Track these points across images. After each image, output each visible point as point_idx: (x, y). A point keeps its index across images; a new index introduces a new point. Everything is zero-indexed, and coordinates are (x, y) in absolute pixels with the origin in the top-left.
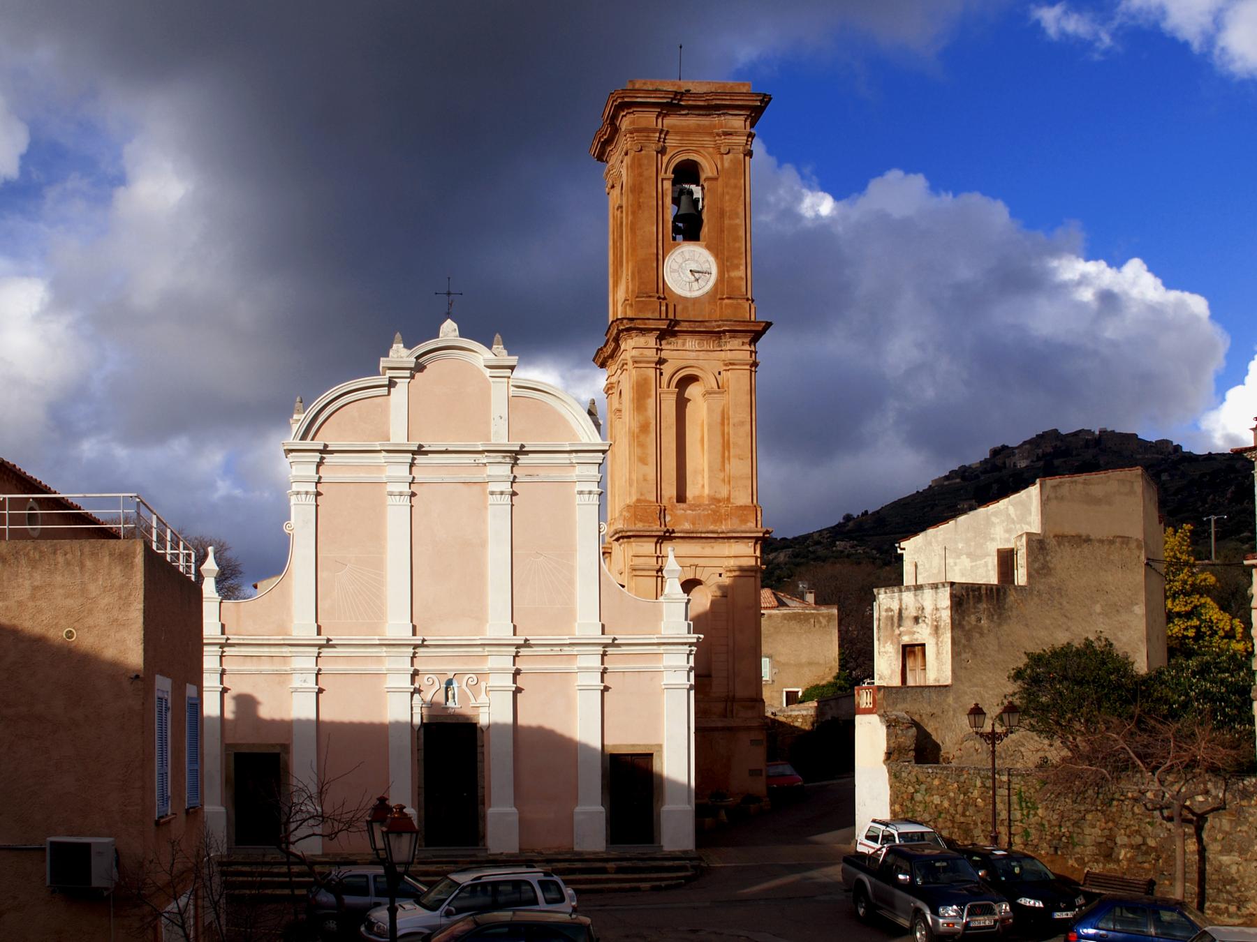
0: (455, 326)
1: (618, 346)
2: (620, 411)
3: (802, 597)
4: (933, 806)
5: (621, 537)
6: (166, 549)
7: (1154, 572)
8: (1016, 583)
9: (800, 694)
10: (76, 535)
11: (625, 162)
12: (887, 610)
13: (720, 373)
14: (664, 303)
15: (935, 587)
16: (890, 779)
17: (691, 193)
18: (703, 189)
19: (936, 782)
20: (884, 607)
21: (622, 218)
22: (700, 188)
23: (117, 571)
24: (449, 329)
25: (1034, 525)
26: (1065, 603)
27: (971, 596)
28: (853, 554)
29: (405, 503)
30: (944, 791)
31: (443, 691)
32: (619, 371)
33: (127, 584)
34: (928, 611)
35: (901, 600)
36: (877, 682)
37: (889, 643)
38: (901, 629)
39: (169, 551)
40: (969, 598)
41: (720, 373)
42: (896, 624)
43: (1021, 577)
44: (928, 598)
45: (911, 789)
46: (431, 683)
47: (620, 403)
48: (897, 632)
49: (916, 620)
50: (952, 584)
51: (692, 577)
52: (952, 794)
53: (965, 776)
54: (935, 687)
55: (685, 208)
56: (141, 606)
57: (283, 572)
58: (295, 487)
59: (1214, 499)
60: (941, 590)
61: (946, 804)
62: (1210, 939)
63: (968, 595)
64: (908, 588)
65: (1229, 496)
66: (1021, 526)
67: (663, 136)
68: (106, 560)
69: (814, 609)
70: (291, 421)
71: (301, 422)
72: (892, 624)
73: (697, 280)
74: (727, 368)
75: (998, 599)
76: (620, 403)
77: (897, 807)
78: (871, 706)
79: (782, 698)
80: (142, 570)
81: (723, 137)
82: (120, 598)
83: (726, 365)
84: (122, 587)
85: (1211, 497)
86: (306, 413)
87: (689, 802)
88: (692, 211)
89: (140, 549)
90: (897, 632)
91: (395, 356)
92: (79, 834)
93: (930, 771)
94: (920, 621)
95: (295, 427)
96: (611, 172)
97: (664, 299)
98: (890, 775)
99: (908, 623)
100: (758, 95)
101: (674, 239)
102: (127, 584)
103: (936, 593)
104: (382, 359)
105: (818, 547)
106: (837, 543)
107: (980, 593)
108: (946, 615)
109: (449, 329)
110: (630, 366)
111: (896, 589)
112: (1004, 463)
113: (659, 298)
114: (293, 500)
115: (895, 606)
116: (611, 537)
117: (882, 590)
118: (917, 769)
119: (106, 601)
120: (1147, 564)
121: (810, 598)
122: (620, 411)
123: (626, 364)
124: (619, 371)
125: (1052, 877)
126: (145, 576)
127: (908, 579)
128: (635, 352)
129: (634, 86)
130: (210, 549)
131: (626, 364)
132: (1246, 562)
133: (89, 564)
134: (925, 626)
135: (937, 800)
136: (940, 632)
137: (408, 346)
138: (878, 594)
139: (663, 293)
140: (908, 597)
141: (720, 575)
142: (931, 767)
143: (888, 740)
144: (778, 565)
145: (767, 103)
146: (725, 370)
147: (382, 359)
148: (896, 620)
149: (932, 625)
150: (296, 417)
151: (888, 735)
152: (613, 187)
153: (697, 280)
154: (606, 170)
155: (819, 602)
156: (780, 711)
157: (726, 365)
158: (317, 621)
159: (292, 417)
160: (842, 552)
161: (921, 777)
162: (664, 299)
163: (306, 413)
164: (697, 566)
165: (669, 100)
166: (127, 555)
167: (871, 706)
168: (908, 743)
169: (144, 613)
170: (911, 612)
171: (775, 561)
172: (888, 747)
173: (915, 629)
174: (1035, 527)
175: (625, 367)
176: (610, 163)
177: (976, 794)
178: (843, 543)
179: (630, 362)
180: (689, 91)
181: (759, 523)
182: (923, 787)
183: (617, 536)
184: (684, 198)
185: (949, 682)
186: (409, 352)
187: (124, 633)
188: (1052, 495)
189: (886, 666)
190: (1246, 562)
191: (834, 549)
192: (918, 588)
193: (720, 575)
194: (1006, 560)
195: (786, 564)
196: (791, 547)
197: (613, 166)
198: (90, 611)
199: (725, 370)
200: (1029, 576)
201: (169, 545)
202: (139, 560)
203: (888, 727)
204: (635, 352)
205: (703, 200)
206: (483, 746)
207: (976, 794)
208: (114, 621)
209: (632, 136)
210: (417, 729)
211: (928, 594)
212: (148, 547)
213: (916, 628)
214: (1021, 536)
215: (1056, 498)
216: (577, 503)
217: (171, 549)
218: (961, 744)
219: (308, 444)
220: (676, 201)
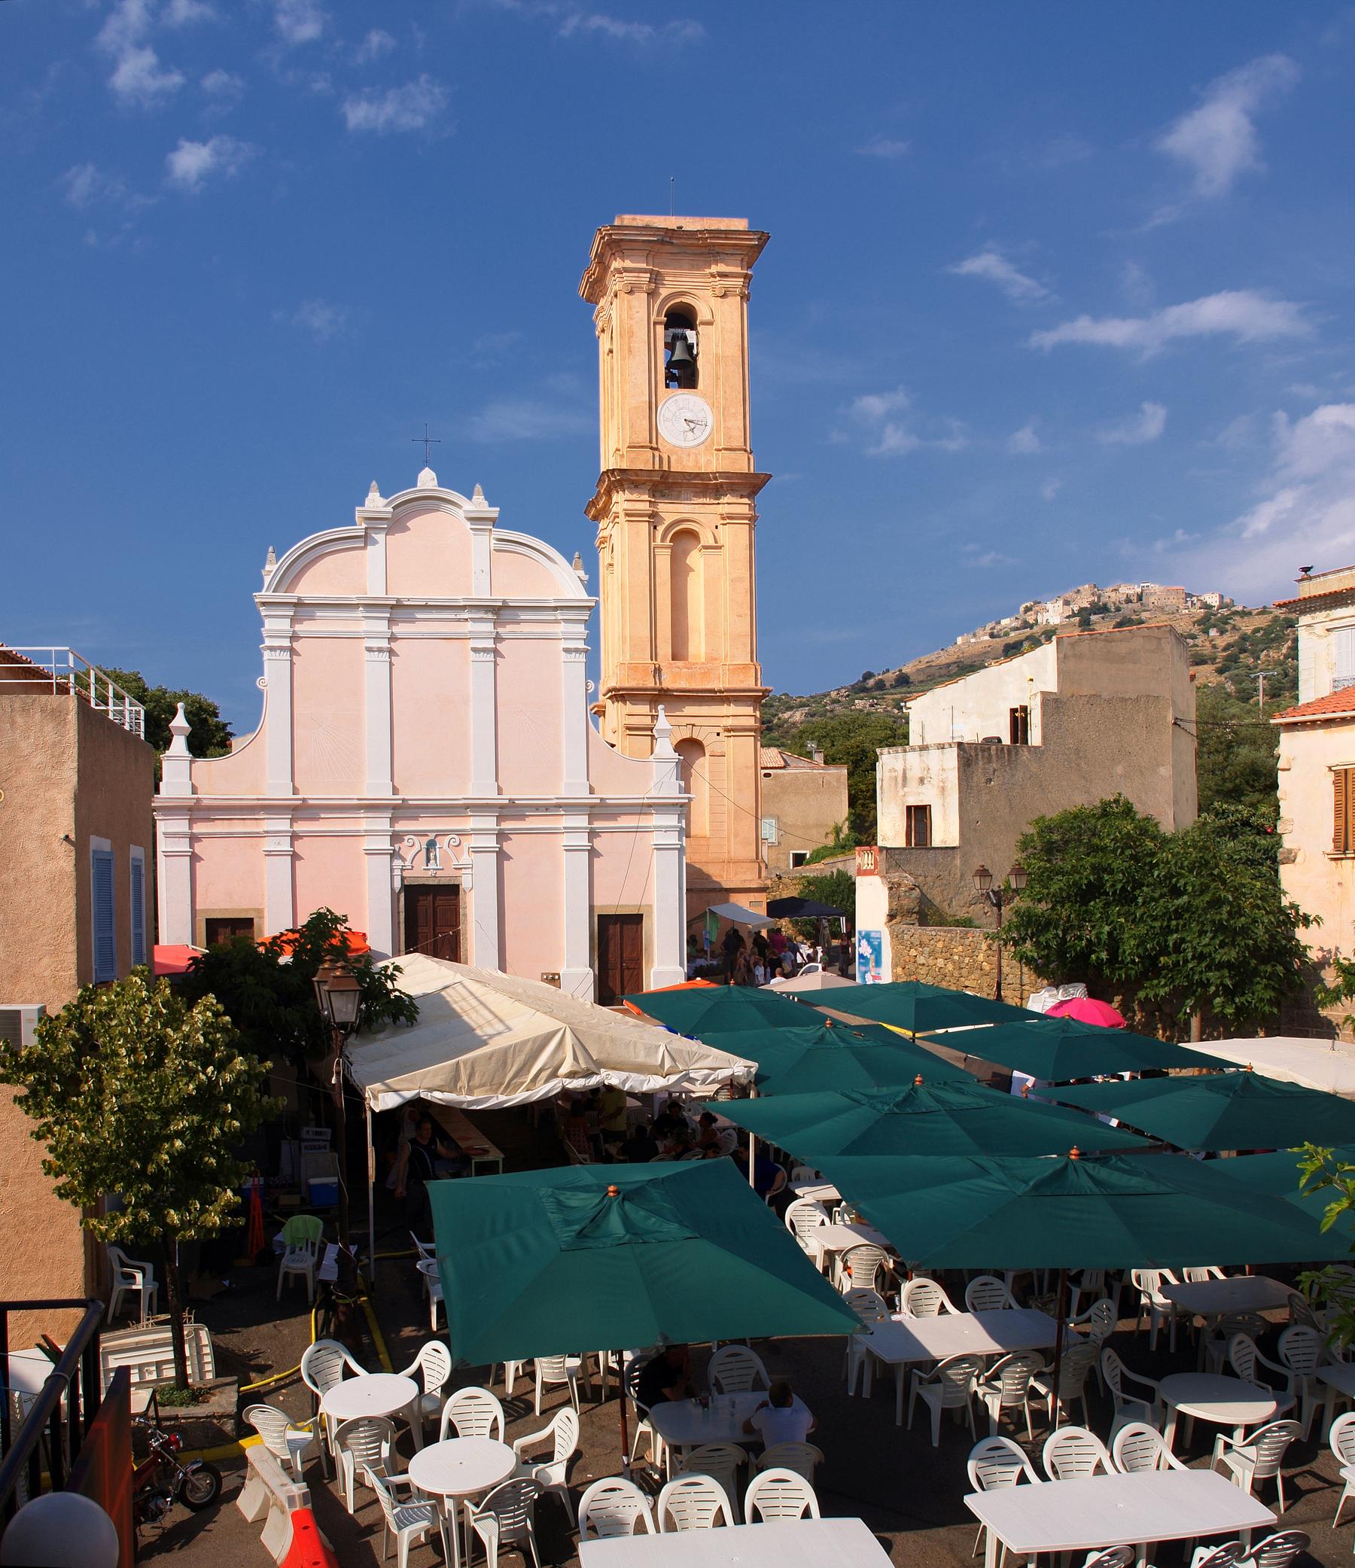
0: (433, 475)
1: (610, 498)
2: (611, 565)
3: (809, 755)
4: (937, 969)
5: (620, 695)
6: (107, 704)
7: (1183, 732)
8: (1030, 744)
9: (808, 856)
10: (27, 689)
11: (614, 304)
12: (890, 771)
13: (717, 527)
14: (657, 453)
15: (942, 747)
16: (892, 941)
17: (685, 338)
18: (697, 334)
19: (940, 945)
20: (887, 768)
21: (612, 363)
22: (694, 332)
23: (49, 728)
24: (427, 479)
25: (1051, 684)
26: (1083, 765)
27: (980, 757)
28: (873, 713)
29: (383, 659)
30: (948, 954)
31: (424, 851)
32: (611, 525)
33: (60, 741)
34: (933, 773)
35: (905, 760)
36: (880, 843)
37: (893, 805)
38: (906, 789)
39: (111, 707)
40: (977, 759)
41: (717, 527)
42: (900, 785)
43: (1035, 737)
44: (933, 756)
45: (913, 952)
46: (410, 844)
47: (612, 558)
48: (901, 793)
49: (922, 781)
50: (960, 744)
51: (688, 736)
52: (956, 957)
53: (971, 939)
54: (941, 848)
55: (679, 354)
56: (76, 764)
57: (255, 730)
58: (268, 642)
59: (1267, 655)
60: (948, 751)
61: (950, 967)
62: (1002, 1417)
63: (977, 755)
64: (913, 749)
65: (1284, 651)
66: (172, 810)
67: (654, 276)
68: (38, 716)
69: (823, 768)
70: (263, 573)
71: (272, 574)
72: (896, 784)
73: (692, 430)
74: (725, 522)
75: (1009, 760)
76: (612, 558)
77: (899, 970)
78: (873, 868)
79: (788, 860)
80: (76, 727)
81: (718, 278)
82: (53, 756)
83: (723, 519)
84: (54, 744)
85: (1265, 652)
86: (279, 564)
87: (681, 964)
88: (687, 357)
89: (71, 702)
90: (901, 793)
91: (372, 506)
92: (9, 1002)
93: (934, 933)
94: (925, 782)
95: (267, 580)
96: (601, 315)
97: (657, 449)
98: (892, 938)
99: (913, 783)
100: (755, 233)
101: (667, 386)
102: (60, 741)
103: (943, 753)
104: (357, 508)
105: (836, 705)
106: (856, 701)
107: (990, 754)
108: (953, 777)
109: (427, 479)
110: (622, 518)
111: (900, 749)
112: (1036, 620)
113: (651, 448)
114: (267, 655)
115: (900, 767)
116: (604, 695)
117: (886, 750)
118: (917, 930)
119: (38, 760)
120: (1175, 723)
121: (819, 758)
122: (611, 565)
123: (618, 517)
124: (611, 525)
125: (666, 1391)
126: (79, 733)
127: (914, 739)
128: (627, 505)
129: (622, 222)
130: (180, 705)
131: (618, 517)
132: (1272, 721)
133: (19, 720)
134: (930, 786)
135: (940, 962)
136: (946, 793)
137: (384, 494)
138: (881, 754)
139: (657, 443)
140: (913, 758)
141: (718, 734)
142: (934, 930)
143: (890, 903)
144: (794, 723)
145: (765, 242)
146: (723, 524)
147: (357, 508)
148: (900, 780)
149: (938, 786)
150: (268, 567)
151: (890, 897)
152: (603, 331)
153: (692, 430)
154: (596, 313)
155: (829, 761)
156: (785, 873)
157: (723, 519)
158: (293, 780)
159: (264, 567)
160: (861, 711)
161: (925, 939)
162: (657, 449)
163: (279, 564)
164: (693, 725)
165: (660, 238)
166: (60, 712)
167: (873, 868)
168: (912, 905)
169: (79, 771)
170: (914, 774)
171: (791, 720)
172: (891, 910)
173: (920, 790)
174: (1052, 687)
175: (616, 520)
176: (600, 305)
177: (981, 957)
178: (863, 702)
179: (622, 515)
180: (681, 227)
181: (759, 682)
182: (927, 950)
183: (610, 694)
184: (679, 345)
185: (956, 843)
186: (386, 501)
187: (54, 793)
188: (1070, 653)
189: (891, 829)
190: (1272, 721)
191: (853, 707)
192: (924, 748)
193: (718, 734)
194: (1019, 721)
195: (801, 723)
196: (808, 706)
197: (602, 307)
198: (18, 770)
199: (723, 524)
200: (1044, 737)
201: (111, 701)
202: (72, 717)
203: (890, 889)
204: (627, 505)
205: (697, 345)
206: (466, 908)
207: (981, 957)
208: (43, 780)
209: (620, 275)
210: (397, 891)
211: (934, 753)
212: (83, 701)
213: (922, 789)
214: (1035, 695)
215: (1075, 655)
216: (562, 660)
217: (114, 706)
218: (969, 907)
219: (282, 596)
220: (670, 346)
